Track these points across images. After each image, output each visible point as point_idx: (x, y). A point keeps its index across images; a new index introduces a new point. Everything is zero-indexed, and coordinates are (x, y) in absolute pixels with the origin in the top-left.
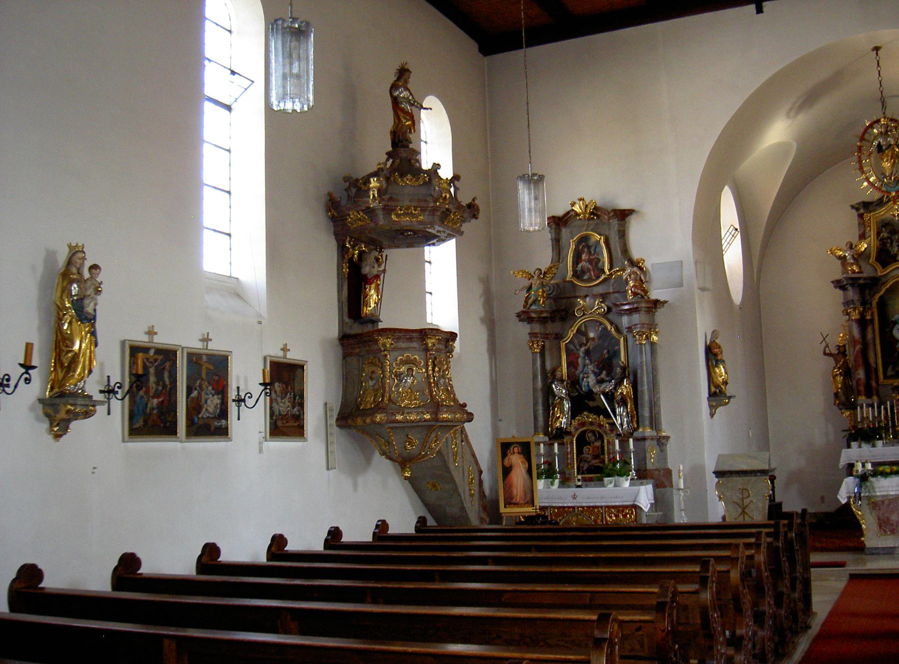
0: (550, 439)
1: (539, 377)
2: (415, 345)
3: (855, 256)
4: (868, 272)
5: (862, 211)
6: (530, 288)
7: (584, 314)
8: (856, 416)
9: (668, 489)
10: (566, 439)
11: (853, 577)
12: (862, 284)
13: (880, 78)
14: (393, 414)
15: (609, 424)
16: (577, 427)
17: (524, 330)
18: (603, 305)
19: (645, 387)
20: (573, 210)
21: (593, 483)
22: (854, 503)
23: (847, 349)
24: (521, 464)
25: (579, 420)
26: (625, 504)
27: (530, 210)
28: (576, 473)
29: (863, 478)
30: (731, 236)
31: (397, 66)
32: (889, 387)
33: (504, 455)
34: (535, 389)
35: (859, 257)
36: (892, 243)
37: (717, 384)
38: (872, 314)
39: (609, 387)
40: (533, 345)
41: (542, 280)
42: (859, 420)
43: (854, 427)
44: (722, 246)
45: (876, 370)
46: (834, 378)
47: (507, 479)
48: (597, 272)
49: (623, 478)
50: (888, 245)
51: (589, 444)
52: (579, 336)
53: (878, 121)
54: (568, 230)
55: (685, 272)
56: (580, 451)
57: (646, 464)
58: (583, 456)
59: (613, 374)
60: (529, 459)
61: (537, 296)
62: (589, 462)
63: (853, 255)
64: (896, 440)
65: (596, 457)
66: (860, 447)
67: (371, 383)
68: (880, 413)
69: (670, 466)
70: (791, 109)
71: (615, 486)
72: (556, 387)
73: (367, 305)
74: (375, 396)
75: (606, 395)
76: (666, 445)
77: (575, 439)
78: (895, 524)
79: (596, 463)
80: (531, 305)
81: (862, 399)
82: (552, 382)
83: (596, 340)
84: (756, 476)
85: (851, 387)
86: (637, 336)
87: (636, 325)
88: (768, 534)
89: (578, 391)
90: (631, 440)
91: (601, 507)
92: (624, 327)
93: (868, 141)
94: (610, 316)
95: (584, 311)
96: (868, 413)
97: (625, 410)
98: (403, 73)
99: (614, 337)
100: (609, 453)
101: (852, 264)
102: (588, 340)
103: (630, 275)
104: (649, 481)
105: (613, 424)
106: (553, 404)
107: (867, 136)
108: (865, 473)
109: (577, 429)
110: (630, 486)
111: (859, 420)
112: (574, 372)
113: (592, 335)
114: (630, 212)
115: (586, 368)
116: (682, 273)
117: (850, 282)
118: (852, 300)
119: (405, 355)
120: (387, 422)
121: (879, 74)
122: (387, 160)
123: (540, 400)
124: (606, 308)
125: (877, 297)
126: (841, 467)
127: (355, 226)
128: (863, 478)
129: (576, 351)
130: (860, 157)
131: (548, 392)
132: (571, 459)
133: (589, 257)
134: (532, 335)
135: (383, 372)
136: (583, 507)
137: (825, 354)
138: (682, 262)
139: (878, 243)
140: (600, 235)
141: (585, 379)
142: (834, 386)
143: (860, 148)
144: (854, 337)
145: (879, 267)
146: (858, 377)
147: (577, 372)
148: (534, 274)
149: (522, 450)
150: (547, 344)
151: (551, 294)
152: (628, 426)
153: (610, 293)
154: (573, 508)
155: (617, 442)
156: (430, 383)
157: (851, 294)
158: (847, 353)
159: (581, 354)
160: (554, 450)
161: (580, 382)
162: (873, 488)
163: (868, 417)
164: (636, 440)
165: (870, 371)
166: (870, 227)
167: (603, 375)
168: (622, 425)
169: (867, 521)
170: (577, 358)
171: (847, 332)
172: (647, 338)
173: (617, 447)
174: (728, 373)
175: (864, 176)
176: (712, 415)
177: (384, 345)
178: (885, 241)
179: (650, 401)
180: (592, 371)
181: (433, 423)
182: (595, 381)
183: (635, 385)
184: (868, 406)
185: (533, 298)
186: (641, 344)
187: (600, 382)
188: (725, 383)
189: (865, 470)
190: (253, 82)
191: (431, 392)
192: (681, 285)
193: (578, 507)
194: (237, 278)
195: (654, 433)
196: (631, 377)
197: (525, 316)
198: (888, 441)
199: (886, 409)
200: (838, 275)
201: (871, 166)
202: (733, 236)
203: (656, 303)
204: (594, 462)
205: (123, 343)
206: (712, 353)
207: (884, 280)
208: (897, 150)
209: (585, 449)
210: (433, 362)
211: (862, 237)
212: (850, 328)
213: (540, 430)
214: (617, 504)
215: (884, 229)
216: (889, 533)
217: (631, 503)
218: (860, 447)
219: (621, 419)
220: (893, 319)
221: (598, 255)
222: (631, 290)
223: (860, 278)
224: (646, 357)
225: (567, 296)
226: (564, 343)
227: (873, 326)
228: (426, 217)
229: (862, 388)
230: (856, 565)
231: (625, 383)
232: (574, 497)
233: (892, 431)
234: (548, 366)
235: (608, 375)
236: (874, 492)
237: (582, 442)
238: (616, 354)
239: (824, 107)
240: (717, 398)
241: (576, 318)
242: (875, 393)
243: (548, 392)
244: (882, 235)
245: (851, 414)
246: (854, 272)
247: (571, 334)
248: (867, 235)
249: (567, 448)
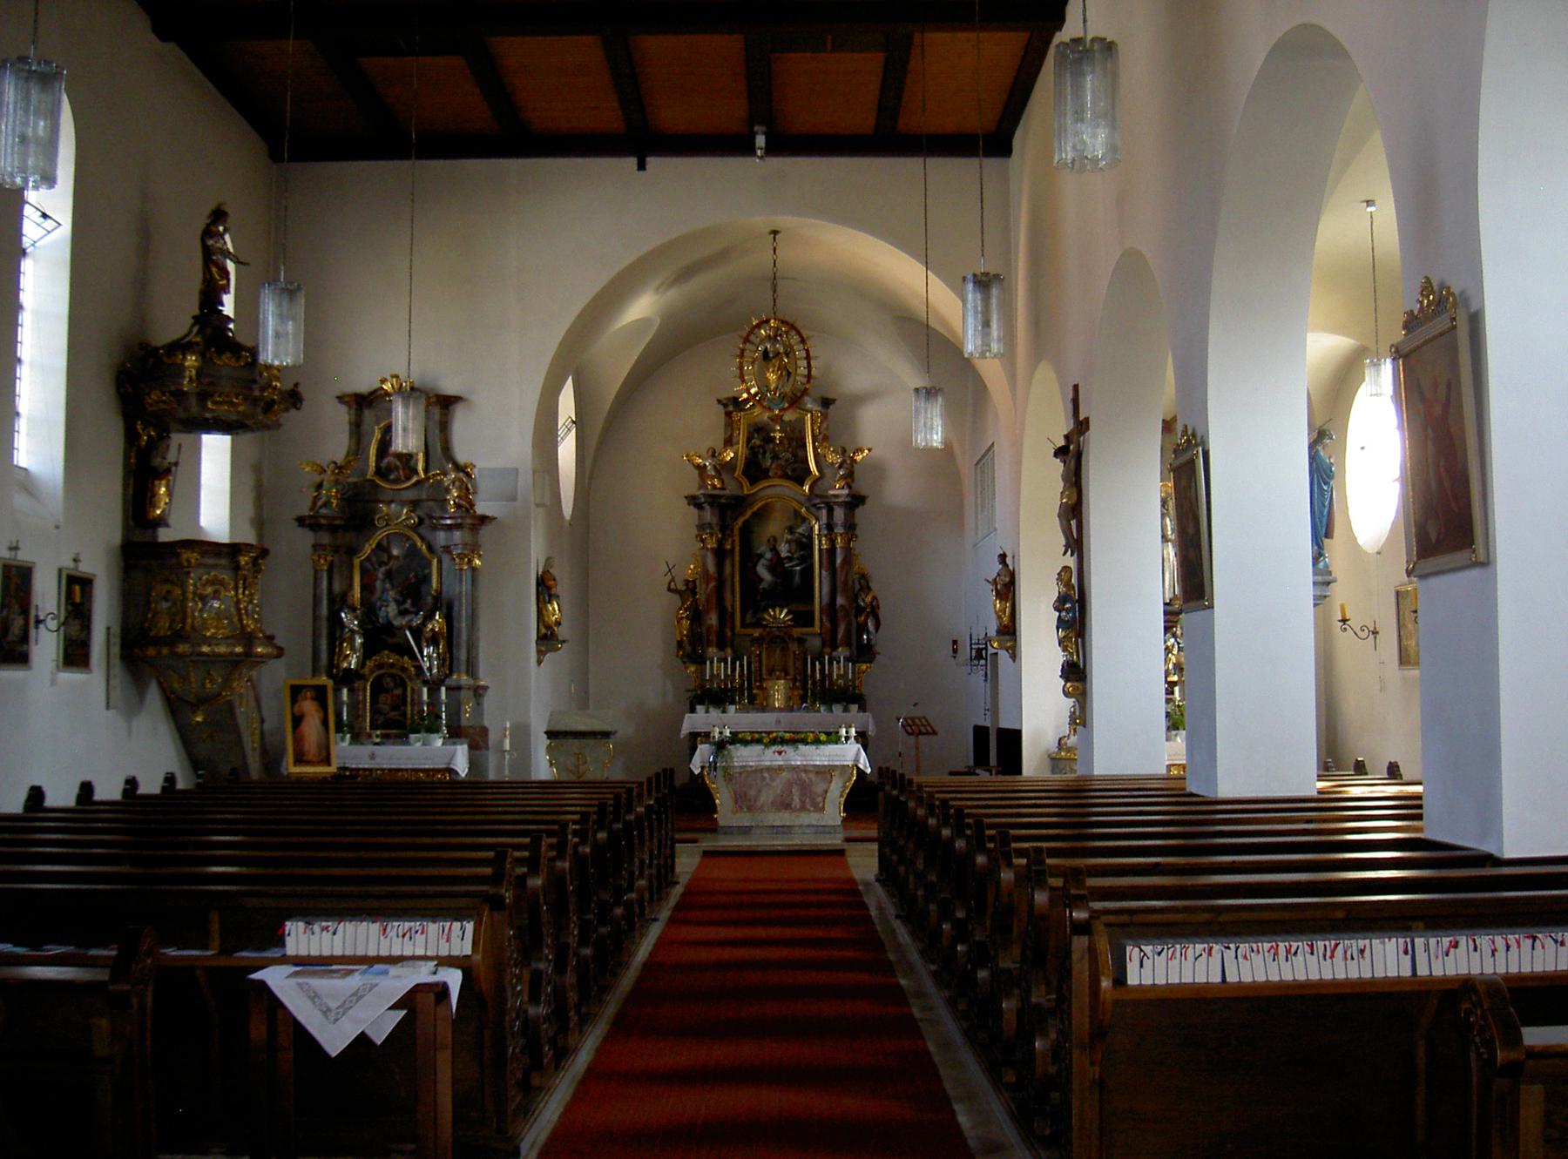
2: (223, 562)
6: (319, 486)
7: (387, 525)
9: (484, 751)
11: (707, 854)
12: (724, 503)
13: (775, 269)
14: (199, 645)
17: (305, 540)
21: (391, 741)
22: (708, 774)
23: (698, 584)
25: (376, 660)
26: (436, 767)
27: (405, 429)
28: (368, 728)
29: (721, 746)
31: (213, 206)
33: (294, 700)
35: (723, 468)
36: (765, 452)
37: (548, 624)
38: (733, 541)
40: (319, 560)
41: (337, 477)
43: (702, 687)
45: (733, 615)
46: (678, 622)
49: (435, 735)
50: (760, 456)
51: (387, 691)
53: (767, 321)
55: (519, 483)
61: (329, 497)
62: (385, 715)
63: (715, 466)
64: (751, 706)
65: (394, 708)
66: (707, 712)
67: (165, 605)
68: (733, 670)
69: (486, 723)
70: (662, 284)
71: (424, 744)
73: (155, 507)
74: (172, 621)
77: (369, 684)
78: (753, 800)
80: (321, 508)
81: (712, 651)
82: (341, 610)
84: (596, 738)
86: (457, 559)
88: (574, 822)
91: (407, 770)
93: (752, 343)
94: (422, 530)
96: (719, 669)
98: (219, 215)
99: (423, 557)
100: (413, 704)
101: (713, 477)
102: (391, 557)
104: (463, 740)
105: (419, 668)
106: (341, 637)
108: (723, 740)
110: (443, 744)
114: (456, 399)
115: (385, 595)
116: (516, 484)
117: (709, 500)
118: (710, 524)
119: (212, 574)
120: (191, 654)
121: (775, 264)
123: (324, 632)
124: (416, 520)
125: (741, 521)
126: (682, 736)
127: (154, 408)
128: (721, 746)
130: (741, 363)
134: (315, 547)
135: (184, 593)
136: (383, 770)
137: (669, 590)
138: (517, 470)
143: (743, 351)
144: (708, 571)
145: (746, 483)
146: (709, 622)
147: (373, 599)
152: (438, 672)
154: (370, 770)
155: (425, 690)
156: (239, 610)
157: (708, 515)
158: (698, 590)
159: (380, 576)
160: (440, 697)
161: (378, 612)
162: (731, 758)
163: (719, 675)
165: (725, 617)
166: (739, 430)
169: (723, 798)
170: (375, 580)
172: (470, 561)
173: (425, 697)
176: (539, 662)
177: (188, 561)
178: (756, 450)
181: (243, 658)
182: (396, 611)
183: (449, 619)
185: (324, 499)
186: (461, 569)
187: (403, 613)
188: (558, 623)
189: (723, 737)
190: (60, 224)
191: (241, 620)
192: (514, 498)
195: (471, 682)
196: (444, 610)
198: (741, 707)
199: (741, 666)
200: (694, 491)
201: (754, 374)
203: (484, 519)
208: (786, 361)
209: (382, 698)
210: (244, 583)
211: (729, 442)
212: (704, 557)
214: (427, 767)
215: (756, 435)
216: (745, 809)
217: (444, 766)
218: (707, 712)
220: (759, 552)
223: (720, 497)
224: (466, 586)
227: (733, 560)
229: (713, 638)
230: (709, 843)
231: (437, 617)
232: (373, 757)
233: (748, 693)
234: (337, 588)
235: (413, 605)
236: (733, 762)
237: (378, 688)
238: (427, 578)
239: (700, 284)
241: (376, 528)
242: (729, 644)
243: (335, 622)
244: (753, 441)
246: (714, 487)
247: (368, 549)
248: (735, 440)
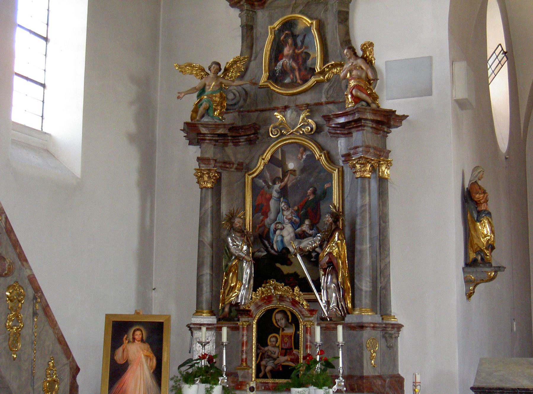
0: (219, 320)
1: (209, 225)
10: (243, 321)
15: (308, 301)
16: (260, 304)
18: (310, 120)
24: (144, 360)
30: (497, 62)
34: (201, 243)
39: (308, 244)
41: (221, 80)
44: (487, 62)
47: (116, 385)
48: (304, 72)
51: (276, 330)
54: (267, 14)
56: (262, 341)
57: (362, 366)
58: (266, 348)
59: (319, 225)
62: (275, 359)
65: (286, 352)
69: (402, 372)
72: (233, 241)
76: (396, 338)
77: (255, 322)
79: (287, 361)
80: (203, 116)
82: (229, 235)
83: (297, 173)
87: (356, 148)
89: (267, 249)
90: (340, 328)
92: (340, 154)
94: (320, 139)
95: (281, 127)
97: (335, 280)
99: (323, 170)
103: (351, 72)
109: (258, 307)
112: (262, 221)
113: (291, 166)
115: (280, 215)
116: (431, 75)
123: (208, 261)
124: (314, 126)
129: (266, 189)
132: (246, 353)
133: (294, 51)
140: (311, 18)
141: (278, 232)
147: (267, 221)
148: (209, 69)
149: (148, 338)
150: (225, 176)
151: (235, 104)
152: (338, 306)
153: (321, 104)
155: (318, 329)
161: (271, 236)
164: (348, 327)
167: (305, 227)
168: (328, 303)
173: (318, 339)
174: (495, 232)
179: (374, 269)
180: (289, 219)
182: (292, 235)
185: (205, 105)
187: (300, 236)
188: (491, 247)
195: (378, 319)
202: (500, 62)
206: (472, 200)
209: (271, 339)
213: (204, 305)
221: (307, 48)
222: (351, 93)
226: (251, 177)
234: (224, 209)
235: (311, 227)
238: (327, 194)
240: (479, 269)
247: (261, 165)
249: (243, 336)
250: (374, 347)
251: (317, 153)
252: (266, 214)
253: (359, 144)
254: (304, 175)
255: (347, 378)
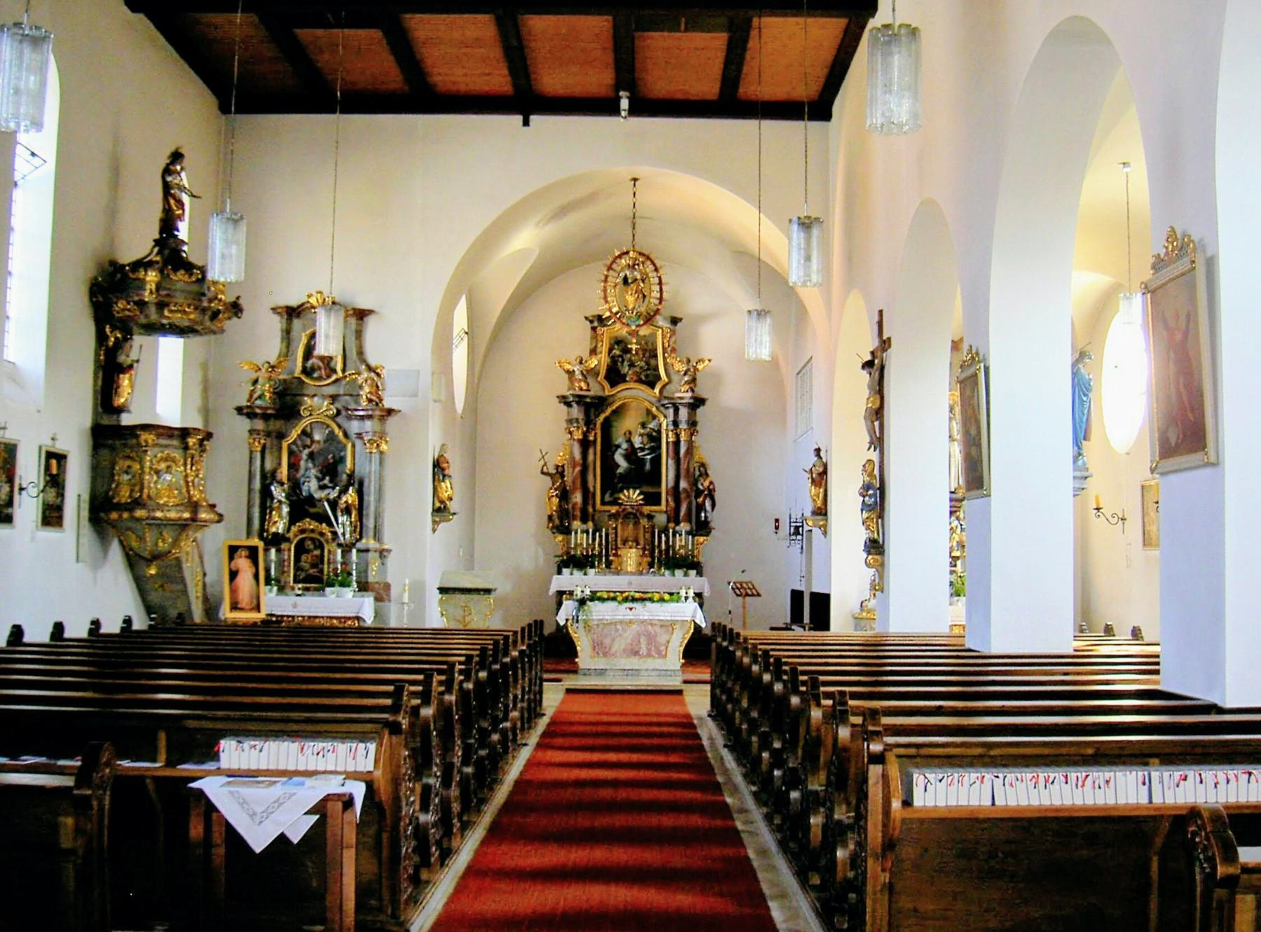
3: (585, 373)
4: (595, 391)
5: (596, 324)
6: (255, 382)
7: (311, 415)
8: (569, 542)
9: (387, 603)
10: (284, 546)
14: (154, 510)
15: (331, 532)
19: (371, 499)
20: (308, 302)
21: (311, 593)
25: (299, 526)
29: (582, 602)
32: (607, 514)
33: (231, 558)
36: (623, 361)
38: (596, 434)
42: (573, 546)
43: (568, 553)
45: (594, 495)
46: (549, 499)
48: (327, 371)
50: (619, 364)
51: (308, 551)
52: (304, 437)
60: (255, 563)
64: (608, 570)
65: (314, 566)
67: (126, 477)
68: (594, 539)
70: (539, 222)
71: (338, 596)
74: (132, 491)
75: (328, 501)
80: (256, 399)
81: (577, 524)
82: (271, 484)
83: (322, 443)
85: (567, 510)
88: (460, 663)
90: (354, 551)
91: (323, 617)
94: (339, 419)
96: (582, 539)
98: (177, 156)
99: (340, 442)
100: (329, 563)
101: (580, 380)
102: (313, 441)
104: (370, 593)
105: (335, 534)
106: (270, 507)
107: (614, 266)
109: (296, 536)
111: (573, 546)
114: (370, 312)
117: (577, 399)
120: (147, 518)
122: (154, 247)
125: (602, 417)
127: (120, 315)
128: (582, 602)
131: (266, 494)
134: (251, 432)
135: (142, 468)
136: (303, 617)
137: (543, 473)
139: (609, 360)
141: (306, 484)
142: (548, 508)
144: (574, 458)
146: (574, 500)
147: (298, 475)
155: (339, 551)
156: (187, 483)
157: (576, 412)
158: (566, 473)
162: (591, 612)
163: (581, 544)
164: (359, 551)
165: (587, 495)
166: (602, 342)
167: (327, 481)
170: (300, 460)
171: (568, 451)
175: (607, 306)
176: (434, 530)
184: (583, 532)
186: (371, 453)
187: (322, 488)
191: (188, 491)
193: (298, 617)
194: (14, 363)
195: (377, 546)
196: (356, 486)
197: (246, 412)
199: (601, 536)
201: (615, 296)
203: (390, 412)
204: (311, 571)
205: (19, 441)
207: (611, 399)
209: (304, 557)
211: (593, 352)
212: (571, 446)
215: (616, 347)
219: (343, 525)
220: (617, 443)
223: (586, 397)
224: (374, 466)
225: (294, 393)
228: (198, 315)
229: (578, 513)
230: (571, 682)
232: (295, 606)
235: (331, 481)
237: (301, 549)
238: (342, 460)
242: (590, 518)
243: (266, 494)
245: (563, 539)
246: (581, 389)
248: (598, 350)
250: (375, 564)
251: (337, 430)
252: (297, 470)
253: (369, 430)
254: (327, 444)
255: (358, 582)
